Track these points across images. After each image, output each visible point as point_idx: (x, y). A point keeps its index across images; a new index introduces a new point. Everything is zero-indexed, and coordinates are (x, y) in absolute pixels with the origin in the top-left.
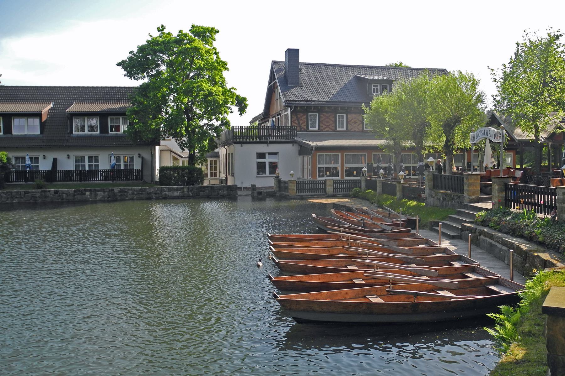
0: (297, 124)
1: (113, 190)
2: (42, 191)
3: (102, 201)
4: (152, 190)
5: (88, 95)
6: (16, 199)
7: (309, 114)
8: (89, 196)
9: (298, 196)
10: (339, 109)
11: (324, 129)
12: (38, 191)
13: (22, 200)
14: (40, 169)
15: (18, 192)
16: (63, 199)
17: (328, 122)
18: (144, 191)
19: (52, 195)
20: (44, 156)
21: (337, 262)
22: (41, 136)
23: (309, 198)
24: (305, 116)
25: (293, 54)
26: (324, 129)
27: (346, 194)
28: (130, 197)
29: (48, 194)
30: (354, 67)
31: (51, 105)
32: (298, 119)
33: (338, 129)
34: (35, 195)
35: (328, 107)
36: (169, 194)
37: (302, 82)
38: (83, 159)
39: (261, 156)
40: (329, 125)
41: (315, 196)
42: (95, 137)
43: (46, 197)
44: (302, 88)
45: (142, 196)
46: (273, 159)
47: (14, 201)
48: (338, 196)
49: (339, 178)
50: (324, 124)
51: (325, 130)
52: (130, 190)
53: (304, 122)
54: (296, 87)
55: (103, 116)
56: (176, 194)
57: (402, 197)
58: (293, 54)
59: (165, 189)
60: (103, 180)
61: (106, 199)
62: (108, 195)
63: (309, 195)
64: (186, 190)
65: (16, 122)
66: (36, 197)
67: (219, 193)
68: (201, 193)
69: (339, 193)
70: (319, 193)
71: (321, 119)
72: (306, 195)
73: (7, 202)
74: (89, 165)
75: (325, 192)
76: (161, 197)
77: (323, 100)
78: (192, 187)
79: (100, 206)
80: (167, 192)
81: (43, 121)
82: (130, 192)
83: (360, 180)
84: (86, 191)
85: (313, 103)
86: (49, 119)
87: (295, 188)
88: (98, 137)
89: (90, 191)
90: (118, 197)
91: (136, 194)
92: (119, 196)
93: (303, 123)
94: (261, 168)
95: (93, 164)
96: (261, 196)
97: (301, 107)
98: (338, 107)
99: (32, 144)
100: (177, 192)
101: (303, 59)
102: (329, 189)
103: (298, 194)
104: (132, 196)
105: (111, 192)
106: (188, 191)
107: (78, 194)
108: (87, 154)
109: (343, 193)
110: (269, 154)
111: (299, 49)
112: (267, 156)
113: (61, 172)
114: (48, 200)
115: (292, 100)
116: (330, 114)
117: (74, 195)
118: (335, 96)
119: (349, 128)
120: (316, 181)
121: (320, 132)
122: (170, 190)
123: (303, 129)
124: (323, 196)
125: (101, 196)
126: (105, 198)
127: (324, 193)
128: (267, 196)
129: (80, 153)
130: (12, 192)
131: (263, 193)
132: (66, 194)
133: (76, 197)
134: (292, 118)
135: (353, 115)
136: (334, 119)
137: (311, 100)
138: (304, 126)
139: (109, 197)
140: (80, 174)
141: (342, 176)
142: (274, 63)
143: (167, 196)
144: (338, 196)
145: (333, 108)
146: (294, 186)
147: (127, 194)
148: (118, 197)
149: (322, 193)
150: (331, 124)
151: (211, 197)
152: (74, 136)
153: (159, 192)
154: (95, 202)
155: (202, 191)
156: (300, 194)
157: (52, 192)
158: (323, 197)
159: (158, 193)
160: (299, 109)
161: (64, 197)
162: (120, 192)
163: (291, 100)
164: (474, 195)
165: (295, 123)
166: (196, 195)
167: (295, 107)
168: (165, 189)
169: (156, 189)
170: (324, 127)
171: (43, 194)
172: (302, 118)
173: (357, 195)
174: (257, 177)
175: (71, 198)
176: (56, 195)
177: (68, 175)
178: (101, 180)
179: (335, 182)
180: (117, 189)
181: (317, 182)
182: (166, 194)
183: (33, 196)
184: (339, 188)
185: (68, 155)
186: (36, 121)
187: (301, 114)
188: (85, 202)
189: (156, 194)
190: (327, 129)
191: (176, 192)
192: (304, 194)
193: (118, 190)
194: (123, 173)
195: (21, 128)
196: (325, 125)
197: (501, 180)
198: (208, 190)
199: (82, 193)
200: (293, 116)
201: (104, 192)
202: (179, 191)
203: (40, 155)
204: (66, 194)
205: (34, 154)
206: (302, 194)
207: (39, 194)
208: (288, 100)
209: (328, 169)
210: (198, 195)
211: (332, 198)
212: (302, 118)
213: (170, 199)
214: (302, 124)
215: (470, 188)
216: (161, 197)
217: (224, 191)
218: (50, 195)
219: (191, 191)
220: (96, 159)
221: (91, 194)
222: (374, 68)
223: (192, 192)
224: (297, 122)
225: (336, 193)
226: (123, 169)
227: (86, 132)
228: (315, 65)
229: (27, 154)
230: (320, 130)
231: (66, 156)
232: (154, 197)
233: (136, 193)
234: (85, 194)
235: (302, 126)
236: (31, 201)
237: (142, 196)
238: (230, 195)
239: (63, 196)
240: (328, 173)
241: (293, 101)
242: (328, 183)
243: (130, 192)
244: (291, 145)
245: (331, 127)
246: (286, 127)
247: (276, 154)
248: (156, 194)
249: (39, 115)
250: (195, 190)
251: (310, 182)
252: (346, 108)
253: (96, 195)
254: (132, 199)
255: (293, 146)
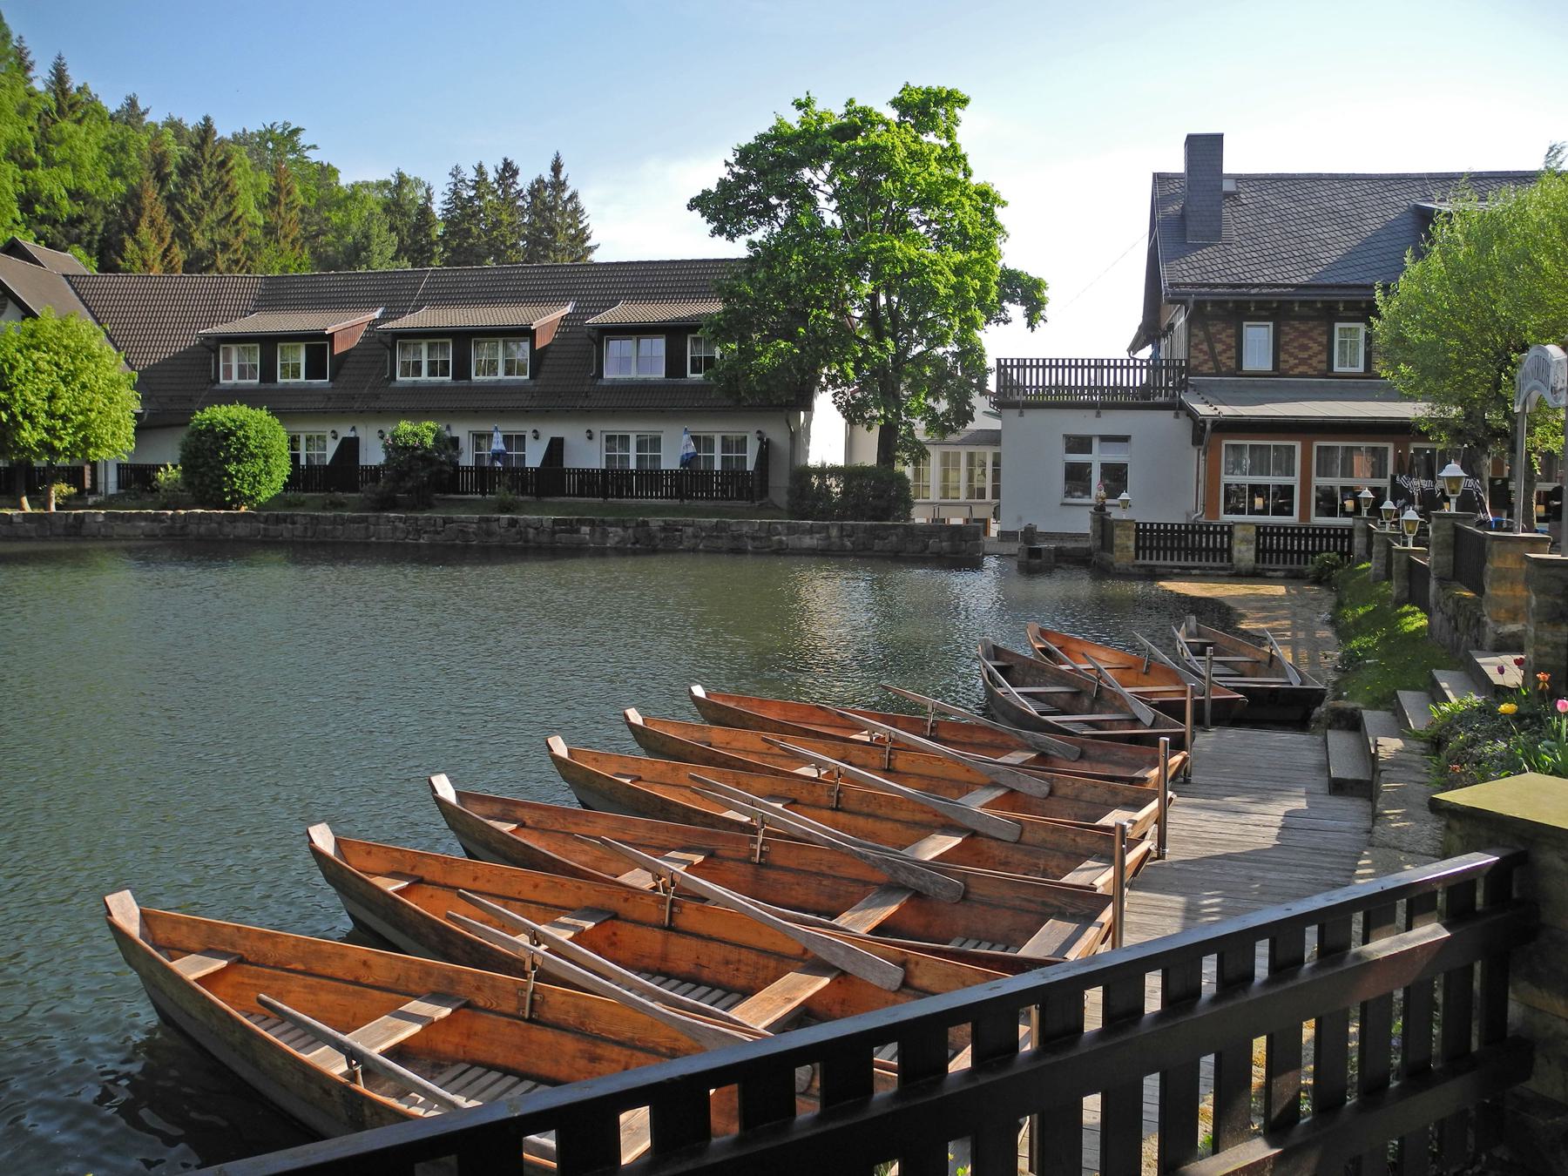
0: (1205, 353)
1: (645, 524)
2: (481, 520)
3: (621, 552)
4: (745, 529)
5: (657, 281)
6: (425, 536)
7: (1338, 326)
8: (587, 537)
9: (1144, 566)
10: (1338, 309)
11: (1292, 368)
12: (473, 518)
13: (438, 537)
14: (528, 465)
15: (430, 518)
16: (527, 541)
17: (1304, 348)
18: (724, 530)
19: (502, 530)
20: (535, 431)
21: (652, 830)
22: (531, 383)
23: (1165, 577)
24: (1231, 331)
25: (1204, 149)
26: (1292, 368)
27: (1298, 570)
28: (686, 544)
29: (494, 526)
30: (1415, 179)
31: (568, 309)
32: (1210, 339)
33: (1337, 369)
34: (466, 527)
35: (1302, 303)
36: (790, 543)
37: (1231, 230)
38: (625, 440)
39: (1079, 444)
40: (1310, 357)
41: (1194, 572)
42: (441, 388)
43: (489, 534)
44: (1228, 247)
45: (720, 543)
46: (1114, 456)
47: (422, 541)
48: (1270, 574)
49: (1293, 520)
50: (1291, 355)
51: (1297, 371)
52: (689, 526)
53: (1229, 348)
54: (1210, 245)
55: (675, 333)
56: (808, 541)
57: (1406, 594)
58: (1204, 149)
59: (779, 526)
60: (672, 497)
61: (629, 546)
62: (635, 536)
63: (1174, 567)
64: (834, 532)
65: (480, 354)
66: (468, 533)
67: (926, 547)
68: (878, 544)
69: (1267, 566)
70: (1211, 564)
71: (1284, 339)
72: (1165, 567)
73: (407, 540)
74: (639, 459)
75: (1230, 559)
76: (769, 547)
77: (1287, 281)
78: (852, 526)
79: (701, 555)
80: (786, 535)
81: (538, 347)
82: (690, 530)
83: (1351, 530)
84: (581, 522)
85: (1254, 291)
86: (555, 343)
87: (1132, 544)
88: (660, 386)
89: (592, 523)
90: (658, 541)
91: (704, 538)
92: (662, 540)
93: (1224, 351)
94: (1077, 477)
95: (648, 454)
96: (1038, 561)
97: (1214, 303)
98: (1337, 302)
99: (510, 404)
100: (811, 538)
101: (1235, 162)
102: (1240, 551)
103: (1140, 562)
104: (693, 541)
105: (640, 529)
106: (841, 537)
107: (562, 531)
108: (634, 430)
109: (1288, 566)
110: (1104, 439)
111: (1222, 135)
112: (1096, 444)
113: (574, 473)
114: (494, 541)
115: (1189, 284)
116: (1311, 324)
117: (554, 533)
118: (1332, 267)
119: (1282, 366)
120: (1215, 526)
121: (1276, 376)
122: (792, 530)
123: (1224, 369)
124: (1221, 572)
125: (617, 539)
126: (626, 544)
127: (1225, 564)
128: (1057, 561)
129: (617, 427)
130: (417, 519)
131: (1044, 553)
132: (536, 529)
133: (557, 536)
134: (1190, 335)
135: (1296, 323)
136: (1324, 339)
137: (1249, 281)
138: (1227, 361)
139: (637, 542)
140: (608, 482)
141: (1305, 514)
142: (1160, 179)
143: (784, 547)
144: (1270, 574)
145: (1231, 305)
146: (1128, 537)
147: (681, 536)
148: (658, 541)
149: (1218, 564)
150: (1316, 355)
151: (904, 554)
152: (604, 383)
153: (763, 535)
154: (601, 553)
155: (878, 537)
156: (1147, 562)
157: (504, 523)
158: (1218, 576)
159: (762, 538)
160: (1209, 308)
161: (531, 536)
162: (663, 529)
163: (1186, 285)
164: (1514, 620)
165: (1201, 351)
166: (861, 547)
167: (1196, 302)
168: (779, 526)
169: (757, 527)
170: (1292, 361)
171: (484, 526)
172: (1223, 337)
173: (1325, 577)
174: (1062, 504)
175: (545, 539)
176: (514, 530)
177: (590, 482)
178: (666, 497)
179: (1262, 532)
180: (656, 522)
181: (1218, 529)
182: (781, 542)
183: (461, 531)
184: (1292, 552)
185: (589, 431)
186: (522, 351)
187: (1220, 326)
188: (576, 551)
189: (754, 539)
190: (1301, 369)
191: (808, 537)
192: (1161, 562)
193: (657, 524)
194: (717, 479)
195: (624, 362)
196: (1296, 358)
197: (1554, 571)
198: (897, 535)
199: (572, 528)
200: (1195, 331)
201: (625, 528)
202: (818, 536)
203: (526, 428)
204: (536, 529)
205: (514, 427)
206: (1154, 562)
207: (474, 526)
208: (1177, 285)
209: (1256, 490)
210: (870, 549)
211: (1248, 580)
212: (1223, 337)
213: (794, 555)
214: (1220, 353)
215: (1500, 593)
216: (769, 547)
217: (941, 541)
218: (497, 529)
219: (848, 536)
220: (656, 443)
221: (592, 533)
222: (1486, 178)
223: (853, 539)
224: (1205, 347)
225: (1267, 566)
226: (719, 469)
227: (501, 375)
228: (1285, 180)
229: (496, 428)
230: (1278, 370)
231: (585, 435)
232: (750, 548)
233: (704, 534)
234: (578, 531)
235: (1223, 358)
236: (457, 542)
237: (720, 543)
238: (957, 553)
239: (527, 533)
240: (1259, 502)
241: (1193, 285)
242: (1238, 533)
243: (690, 530)
244: (1171, 413)
245: (1314, 362)
246: (1175, 361)
247: (1125, 439)
248: (754, 539)
249: (526, 333)
250: (860, 535)
251: (1194, 526)
252: (1275, 305)
253: (605, 535)
254: (693, 550)
255: (1177, 416)
